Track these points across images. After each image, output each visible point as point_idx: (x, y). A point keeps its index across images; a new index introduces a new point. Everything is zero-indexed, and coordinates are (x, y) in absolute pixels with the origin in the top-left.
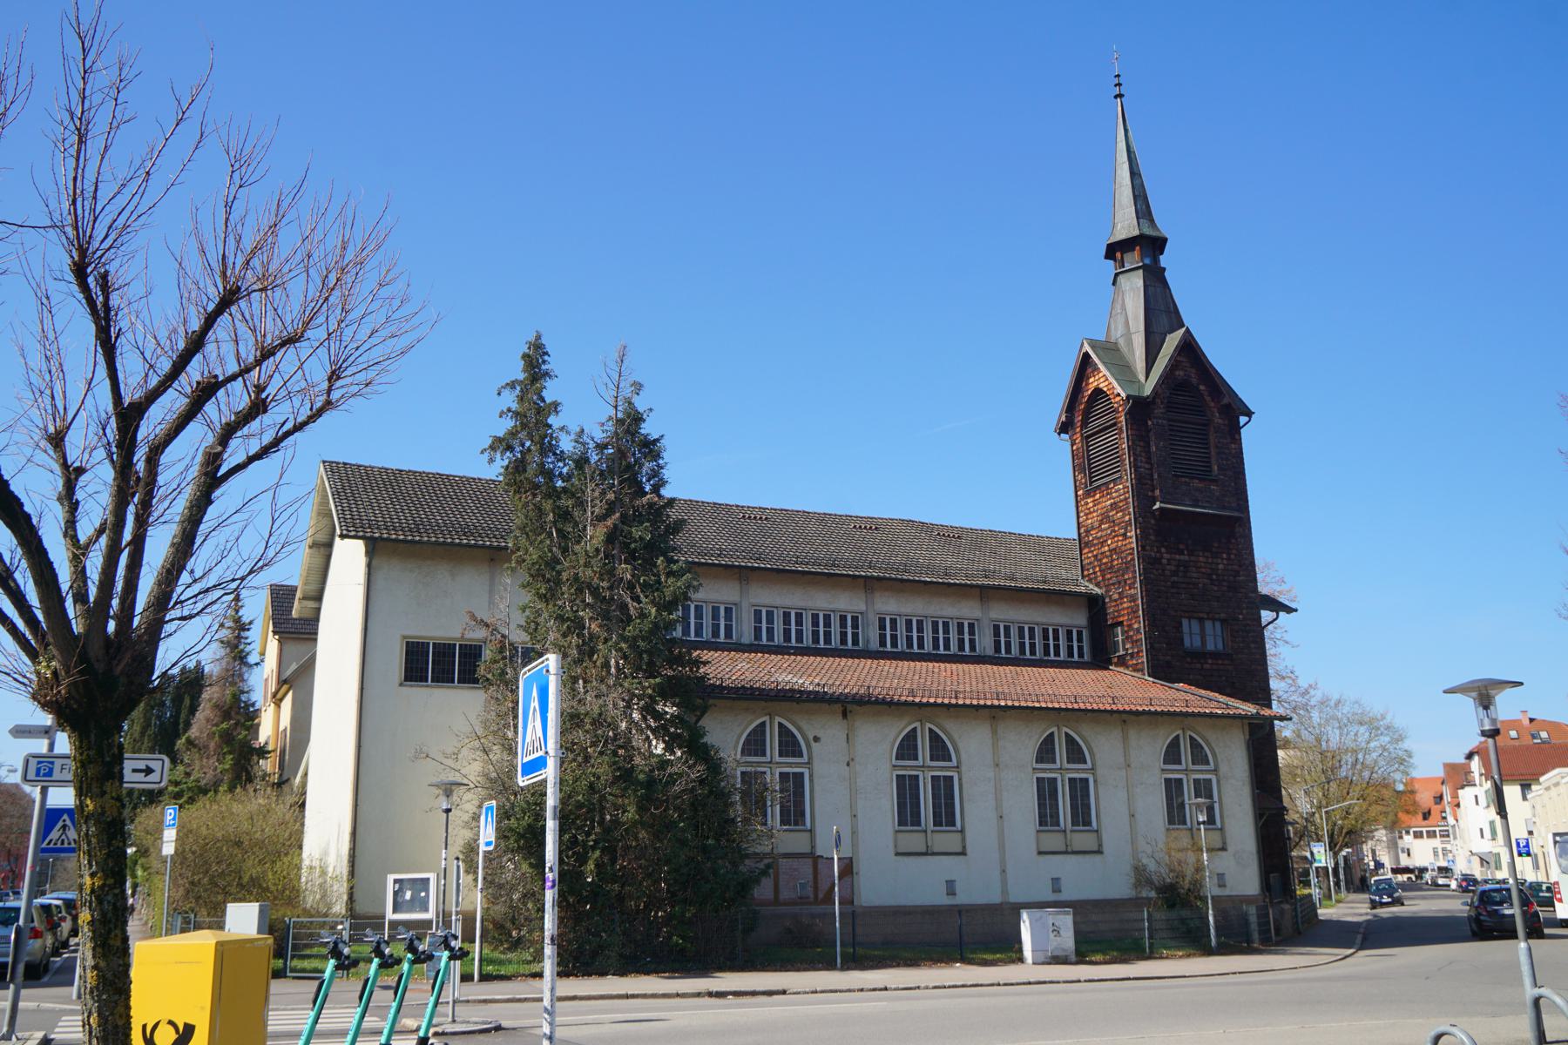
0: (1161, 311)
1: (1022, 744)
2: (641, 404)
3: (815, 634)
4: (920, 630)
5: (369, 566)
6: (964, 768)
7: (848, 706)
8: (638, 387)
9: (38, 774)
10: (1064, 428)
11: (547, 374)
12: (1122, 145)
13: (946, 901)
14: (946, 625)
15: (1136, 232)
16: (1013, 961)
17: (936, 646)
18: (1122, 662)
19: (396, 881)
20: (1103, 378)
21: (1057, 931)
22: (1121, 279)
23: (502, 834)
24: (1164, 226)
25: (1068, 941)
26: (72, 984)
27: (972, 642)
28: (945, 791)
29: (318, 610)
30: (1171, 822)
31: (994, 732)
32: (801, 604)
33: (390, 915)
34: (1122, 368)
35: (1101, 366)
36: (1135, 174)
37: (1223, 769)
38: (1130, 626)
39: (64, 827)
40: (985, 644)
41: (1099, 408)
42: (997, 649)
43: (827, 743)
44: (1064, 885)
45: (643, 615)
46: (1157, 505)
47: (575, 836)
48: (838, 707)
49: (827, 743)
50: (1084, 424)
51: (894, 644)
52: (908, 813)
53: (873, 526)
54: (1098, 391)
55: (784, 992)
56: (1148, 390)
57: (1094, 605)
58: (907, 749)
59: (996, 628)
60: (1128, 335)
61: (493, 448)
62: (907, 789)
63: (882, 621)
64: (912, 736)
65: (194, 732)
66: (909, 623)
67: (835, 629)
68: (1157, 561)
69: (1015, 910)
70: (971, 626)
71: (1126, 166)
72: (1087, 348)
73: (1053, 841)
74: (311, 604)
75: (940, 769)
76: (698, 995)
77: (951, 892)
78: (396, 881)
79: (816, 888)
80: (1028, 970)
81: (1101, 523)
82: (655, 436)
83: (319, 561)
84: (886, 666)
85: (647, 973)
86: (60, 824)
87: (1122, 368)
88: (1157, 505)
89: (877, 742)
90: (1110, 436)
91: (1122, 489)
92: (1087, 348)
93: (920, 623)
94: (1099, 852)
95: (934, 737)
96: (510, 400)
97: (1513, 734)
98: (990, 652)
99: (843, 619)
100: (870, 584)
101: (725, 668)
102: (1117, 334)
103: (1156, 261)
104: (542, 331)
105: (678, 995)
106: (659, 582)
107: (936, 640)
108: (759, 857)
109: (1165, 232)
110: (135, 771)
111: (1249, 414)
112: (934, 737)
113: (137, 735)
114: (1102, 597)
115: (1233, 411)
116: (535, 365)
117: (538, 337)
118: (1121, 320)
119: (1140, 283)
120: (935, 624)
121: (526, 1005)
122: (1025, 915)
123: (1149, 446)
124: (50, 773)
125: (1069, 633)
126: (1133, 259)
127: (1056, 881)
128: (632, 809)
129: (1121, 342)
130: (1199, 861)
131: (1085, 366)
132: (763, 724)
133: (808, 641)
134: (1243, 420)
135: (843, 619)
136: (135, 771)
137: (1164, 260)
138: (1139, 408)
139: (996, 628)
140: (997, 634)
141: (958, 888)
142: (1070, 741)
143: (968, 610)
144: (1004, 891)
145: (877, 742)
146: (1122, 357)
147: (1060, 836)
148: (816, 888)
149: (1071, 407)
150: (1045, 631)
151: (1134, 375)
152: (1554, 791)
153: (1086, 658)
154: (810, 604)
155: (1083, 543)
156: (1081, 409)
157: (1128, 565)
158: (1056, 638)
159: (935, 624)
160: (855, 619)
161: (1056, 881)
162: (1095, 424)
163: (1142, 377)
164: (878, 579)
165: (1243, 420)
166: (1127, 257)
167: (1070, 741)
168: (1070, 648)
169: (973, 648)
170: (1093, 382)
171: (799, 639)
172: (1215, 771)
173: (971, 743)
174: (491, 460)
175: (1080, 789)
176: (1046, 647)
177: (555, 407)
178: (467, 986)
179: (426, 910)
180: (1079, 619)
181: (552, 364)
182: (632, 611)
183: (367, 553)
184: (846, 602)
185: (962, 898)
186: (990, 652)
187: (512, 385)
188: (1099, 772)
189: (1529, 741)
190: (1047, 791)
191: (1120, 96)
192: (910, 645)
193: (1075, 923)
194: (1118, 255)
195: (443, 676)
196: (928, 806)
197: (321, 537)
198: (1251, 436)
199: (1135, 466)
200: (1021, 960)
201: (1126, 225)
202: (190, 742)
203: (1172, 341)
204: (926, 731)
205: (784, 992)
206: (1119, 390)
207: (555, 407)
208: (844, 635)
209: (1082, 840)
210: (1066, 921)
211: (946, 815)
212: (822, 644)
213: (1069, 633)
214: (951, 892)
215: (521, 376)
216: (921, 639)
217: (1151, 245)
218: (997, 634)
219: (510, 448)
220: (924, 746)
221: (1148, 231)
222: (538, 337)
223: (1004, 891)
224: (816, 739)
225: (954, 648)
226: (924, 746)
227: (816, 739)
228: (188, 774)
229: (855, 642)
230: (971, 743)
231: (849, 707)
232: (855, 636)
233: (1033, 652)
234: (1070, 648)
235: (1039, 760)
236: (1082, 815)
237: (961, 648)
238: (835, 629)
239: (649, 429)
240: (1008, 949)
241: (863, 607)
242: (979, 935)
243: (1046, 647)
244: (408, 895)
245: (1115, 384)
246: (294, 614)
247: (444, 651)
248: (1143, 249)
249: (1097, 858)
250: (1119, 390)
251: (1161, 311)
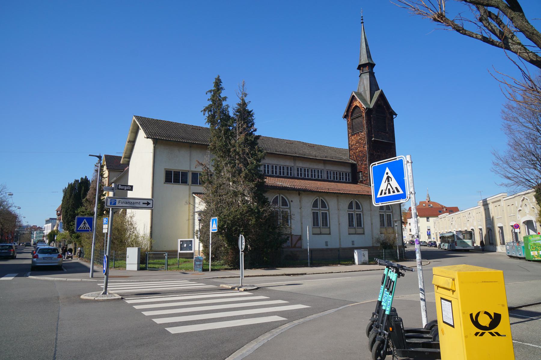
0: (374, 86)
1: (344, 204)
2: (247, 100)
3: (273, 171)
4: (308, 172)
5: (154, 147)
6: (330, 210)
7: (300, 192)
8: (246, 95)
9: (111, 204)
10: (345, 117)
11: (222, 88)
12: (363, 37)
13: (325, 247)
14: (314, 171)
15: (367, 62)
16: (351, 264)
17: (312, 177)
18: (362, 182)
19: (181, 241)
20: (358, 102)
21: (364, 256)
22: (362, 75)
23: (220, 228)
24: (375, 61)
25: (366, 258)
26: (89, 272)
27: (321, 175)
28: (325, 216)
29: (129, 161)
30: (381, 226)
31: (338, 200)
32: (276, 163)
33: (179, 251)
34: (364, 100)
35: (358, 99)
36: (367, 45)
37: (394, 211)
38: (364, 172)
39: (85, 223)
40: (325, 176)
41: (356, 111)
42: (328, 178)
43: (295, 202)
44: (355, 243)
45: (252, 163)
46: (373, 139)
47: (237, 228)
48: (297, 192)
49: (295, 202)
50: (352, 115)
51: (301, 176)
52: (315, 223)
53: (291, 143)
54: (356, 106)
55: (306, 274)
56: (371, 106)
57: (353, 167)
58: (315, 205)
59: (328, 172)
60: (365, 91)
61: (205, 110)
62: (315, 216)
63: (298, 169)
64: (316, 200)
65: (88, 197)
66: (305, 170)
67: (285, 171)
68: (373, 154)
69: (352, 250)
70: (321, 171)
71: (364, 43)
72: (354, 94)
73: (352, 231)
74: (127, 160)
75: (324, 210)
76: (283, 275)
77: (327, 245)
78: (181, 241)
79: (292, 244)
80: (357, 266)
81: (356, 143)
82: (250, 110)
83: (130, 147)
84: (302, 181)
85: (257, 268)
86: (83, 222)
87: (364, 100)
88: (373, 139)
89: (308, 202)
90: (360, 119)
91: (363, 134)
92: (354, 94)
93: (308, 170)
94: (364, 234)
95: (322, 201)
96: (209, 96)
97: (424, 205)
98: (326, 178)
99: (288, 168)
100: (295, 158)
101: (269, 181)
102: (361, 90)
103: (372, 70)
104: (220, 75)
105: (277, 275)
106: (255, 153)
107: (312, 175)
108: (286, 234)
109: (375, 63)
110: (143, 203)
111: (396, 115)
112: (322, 201)
113: (68, 198)
114: (356, 164)
115: (393, 114)
116: (218, 83)
117: (219, 77)
118: (362, 87)
119: (368, 76)
120: (312, 170)
121: (274, 277)
122: (356, 251)
123: (371, 122)
124: (115, 204)
125: (346, 174)
126: (366, 69)
127: (353, 242)
128: (254, 220)
129: (363, 93)
130: (395, 236)
131: (353, 99)
132: (277, 197)
133: (278, 174)
134: (394, 116)
135: (288, 168)
136: (143, 203)
137: (375, 70)
138: (369, 111)
139: (328, 172)
140: (328, 174)
141: (329, 244)
142: (357, 203)
143: (320, 167)
144: (340, 245)
145: (308, 202)
146: (363, 97)
147: (354, 229)
148: (292, 244)
149: (348, 111)
150: (340, 173)
151: (367, 102)
152: (443, 219)
153: (350, 181)
154: (279, 163)
155: (350, 149)
156: (351, 112)
157: (364, 156)
158: (343, 175)
159: (312, 170)
160: (291, 168)
161: (353, 242)
162: (355, 116)
163: (369, 103)
164: (298, 157)
165: (394, 116)
166: (364, 69)
167: (357, 203)
168: (346, 178)
169: (321, 177)
170: (356, 103)
171: (276, 173)
172: (392, 212)
173: (332, 203)
174: (204, 114)
175: (359, 217)
176: (340, 178)
177: (225, 99)
178: (206, 273)
179: (192, 250)
180: (348, 170)
181: (223, 85)
182: (249, 162)
183: (154, 143)
184: (288, 163)
185: (330, 247)
186: (326, 178)
187: (211, 91)
188: (364, 212)
189: (428, 207)
190: (350, 216)
191: (363, 23)
192: (305, 176)
193: (369, 253)
194: (362, 68)
195: (177, 181)
196: (320, 221)
197: (132, 140)
198: (396, 121)
199: (367, 127)
200: (354, 263)
201: (364, 60)
202: (87, 200)
203: (377, 94)
204: (320, 199)
205: (306, 274)
206: (364, 106)
207: (225, 99)
208: (280, 172)
209: (359, 231)
210: (366, 253)
211: (325, 223)
212: (282, 175)
213: (346, 174)
214: (327, 245)
215: (213, 88)
216: (308, 174)
217: (371, 65)
218: (328, 174)
219: (211, 111)
220: (319, 203)
221: (371, 62)
222: (219, 77)
223: (340, 245)
224: (292, 201)
225: (316, 177)
226: (319, 203)
227: (292, 201)
228: (86, 209)
229: (291, 175)
230: (332, 203)
231: (300, 192)
232: (291, 173)
233: (337, 179)
234: (346, 178)
235: (349, 208)
236: (359, 224)
237: (318, 177)
238: (285, 171)
239: (249, 108)
240: (350, 260)
241: (293, 165)
242: (343, 257)
243: (340, 178)
244: (185, 245)
245: (363, 104)
246: (121, 162)
247: (177, 173)
248: (368, 67)
249: (363, 236)
250: (364, 106)
251: (374, 86)
